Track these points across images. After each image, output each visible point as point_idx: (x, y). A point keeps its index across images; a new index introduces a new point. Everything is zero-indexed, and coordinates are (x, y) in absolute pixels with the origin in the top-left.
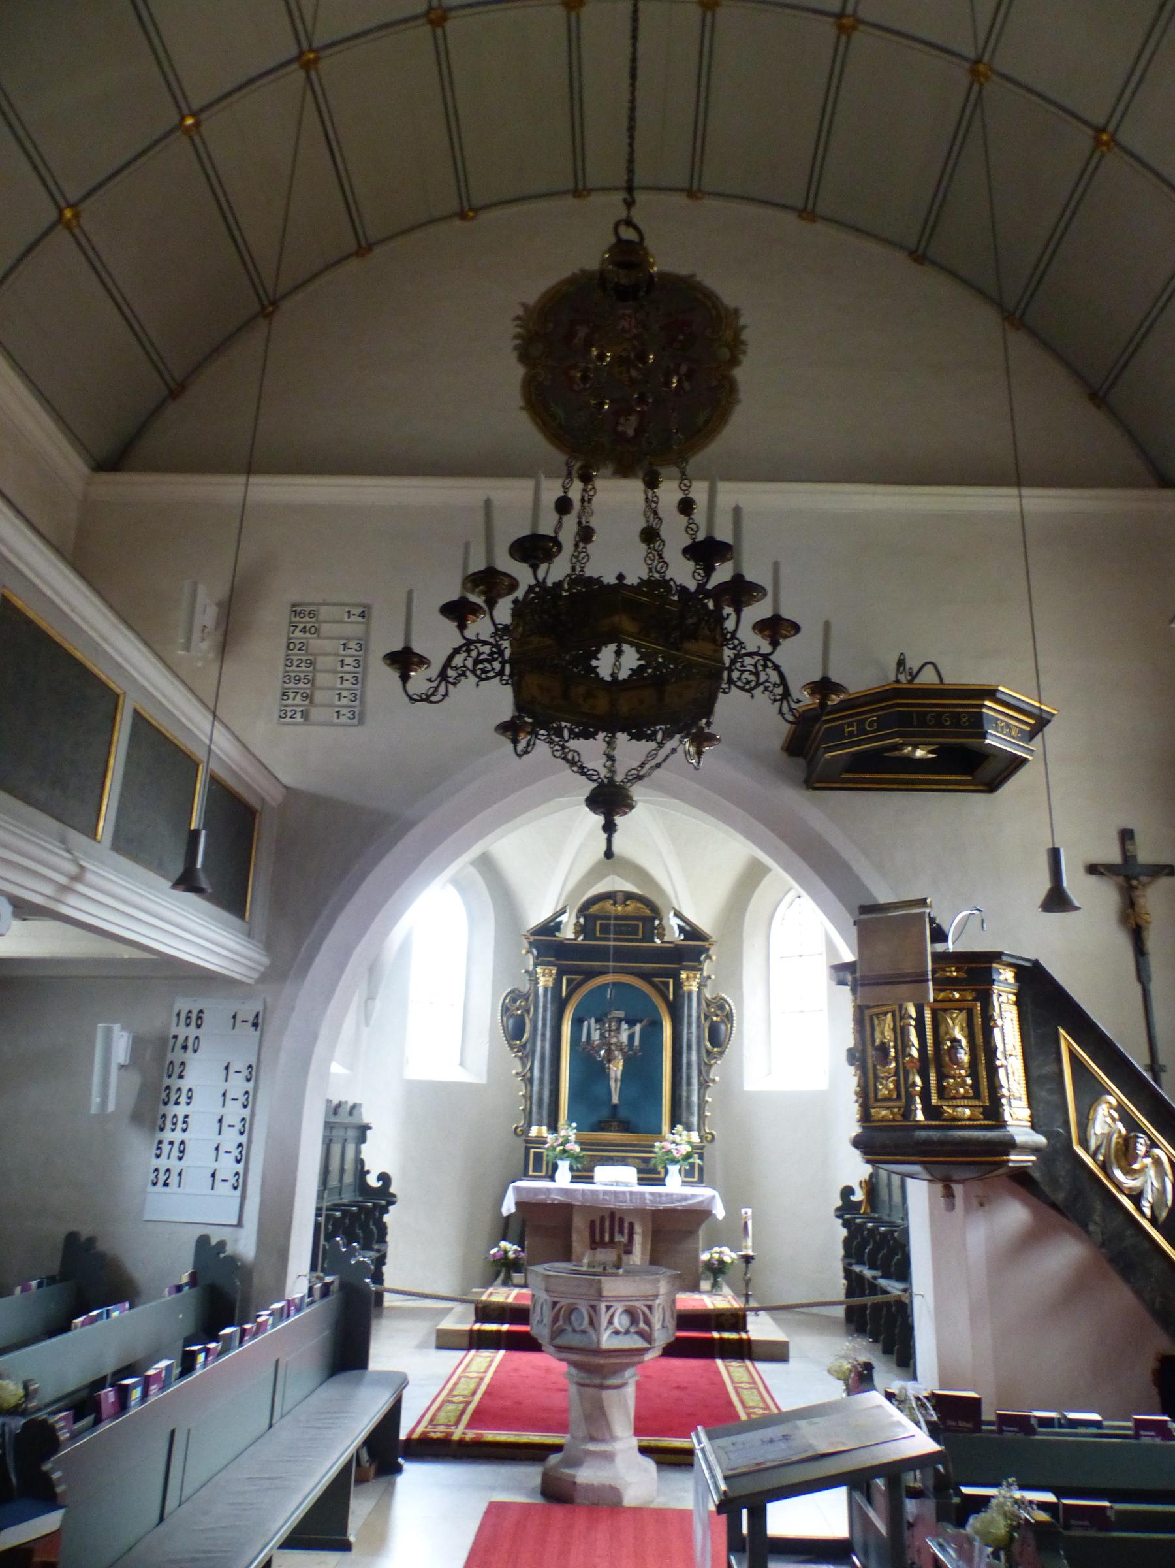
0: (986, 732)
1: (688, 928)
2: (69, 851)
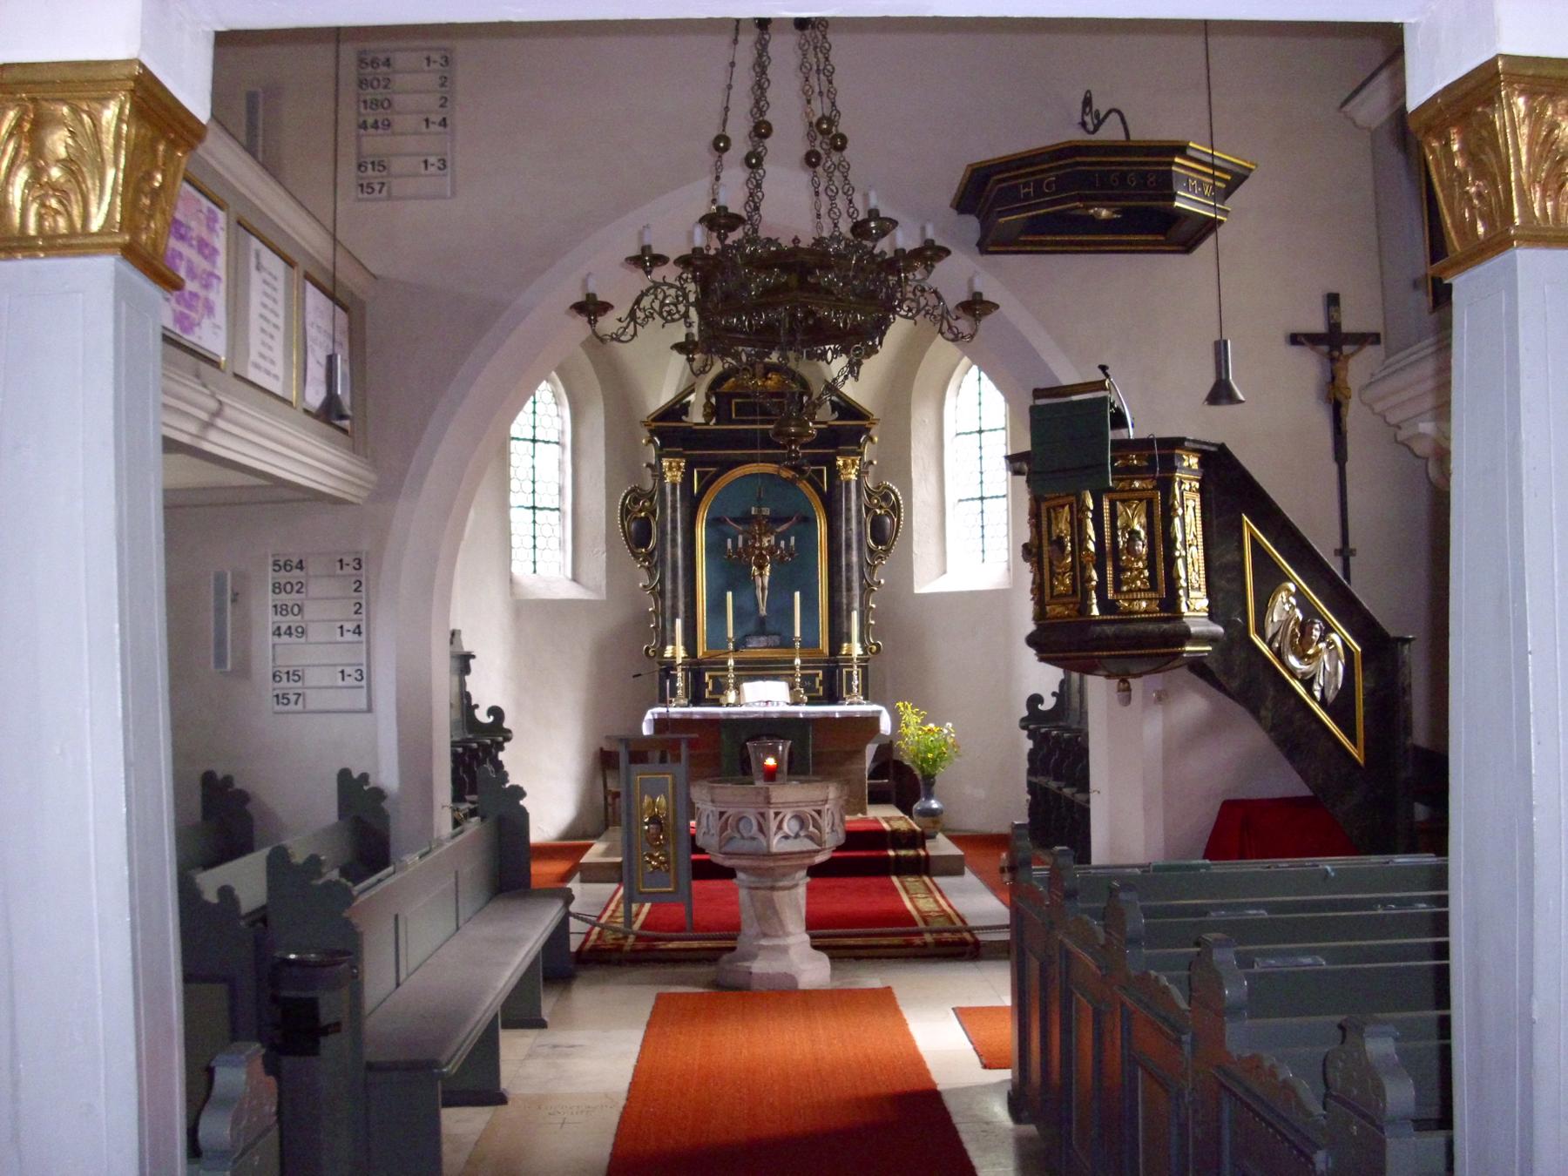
0: (1176, 193)
1: (843, 404)
2: (205, 386)
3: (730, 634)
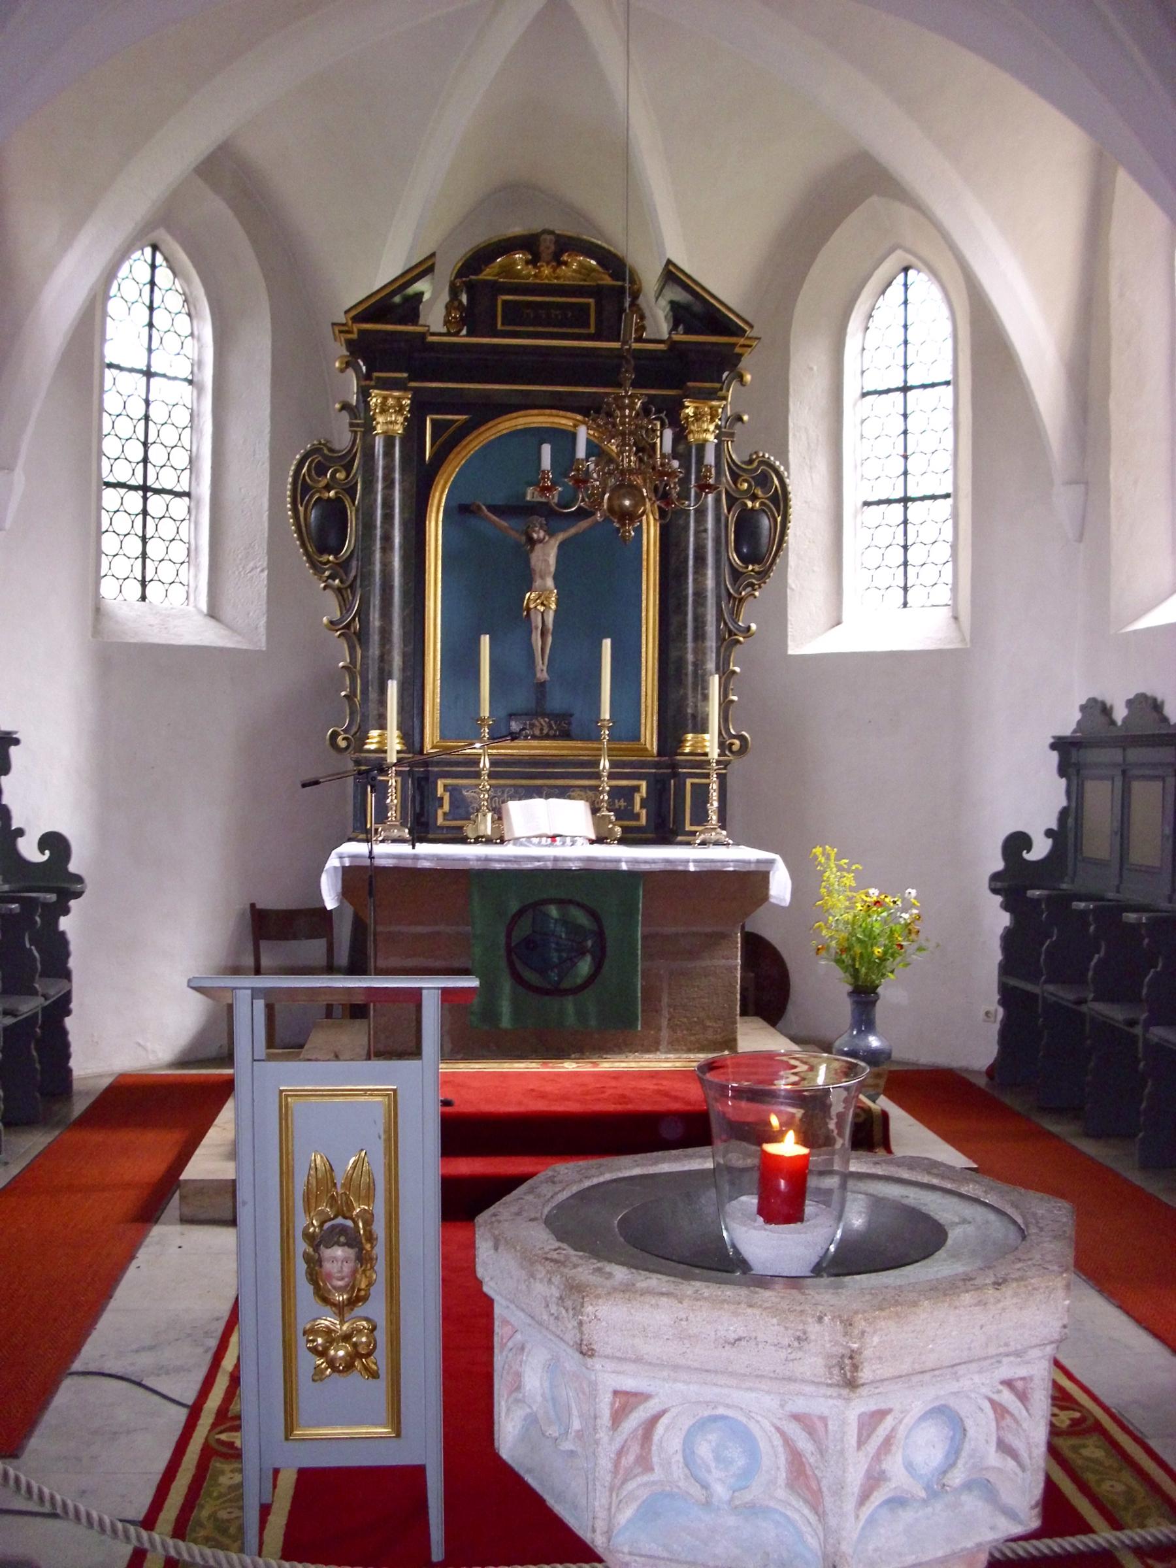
1: (698, 308)
3: (485, 712)
